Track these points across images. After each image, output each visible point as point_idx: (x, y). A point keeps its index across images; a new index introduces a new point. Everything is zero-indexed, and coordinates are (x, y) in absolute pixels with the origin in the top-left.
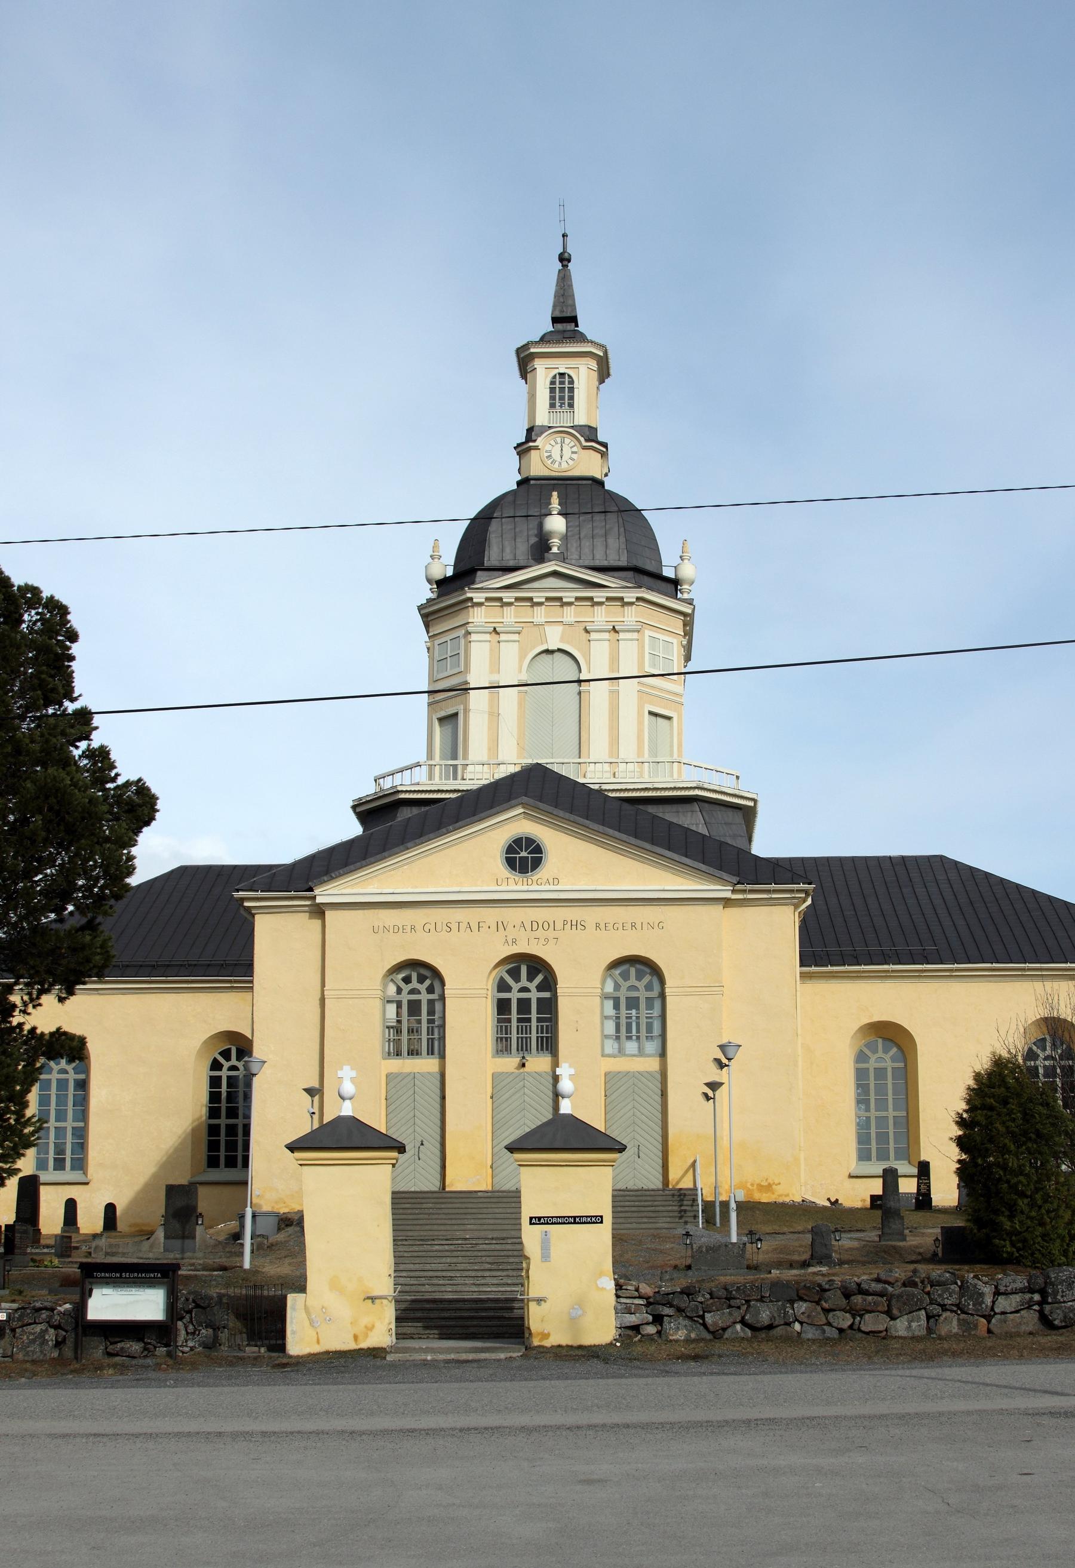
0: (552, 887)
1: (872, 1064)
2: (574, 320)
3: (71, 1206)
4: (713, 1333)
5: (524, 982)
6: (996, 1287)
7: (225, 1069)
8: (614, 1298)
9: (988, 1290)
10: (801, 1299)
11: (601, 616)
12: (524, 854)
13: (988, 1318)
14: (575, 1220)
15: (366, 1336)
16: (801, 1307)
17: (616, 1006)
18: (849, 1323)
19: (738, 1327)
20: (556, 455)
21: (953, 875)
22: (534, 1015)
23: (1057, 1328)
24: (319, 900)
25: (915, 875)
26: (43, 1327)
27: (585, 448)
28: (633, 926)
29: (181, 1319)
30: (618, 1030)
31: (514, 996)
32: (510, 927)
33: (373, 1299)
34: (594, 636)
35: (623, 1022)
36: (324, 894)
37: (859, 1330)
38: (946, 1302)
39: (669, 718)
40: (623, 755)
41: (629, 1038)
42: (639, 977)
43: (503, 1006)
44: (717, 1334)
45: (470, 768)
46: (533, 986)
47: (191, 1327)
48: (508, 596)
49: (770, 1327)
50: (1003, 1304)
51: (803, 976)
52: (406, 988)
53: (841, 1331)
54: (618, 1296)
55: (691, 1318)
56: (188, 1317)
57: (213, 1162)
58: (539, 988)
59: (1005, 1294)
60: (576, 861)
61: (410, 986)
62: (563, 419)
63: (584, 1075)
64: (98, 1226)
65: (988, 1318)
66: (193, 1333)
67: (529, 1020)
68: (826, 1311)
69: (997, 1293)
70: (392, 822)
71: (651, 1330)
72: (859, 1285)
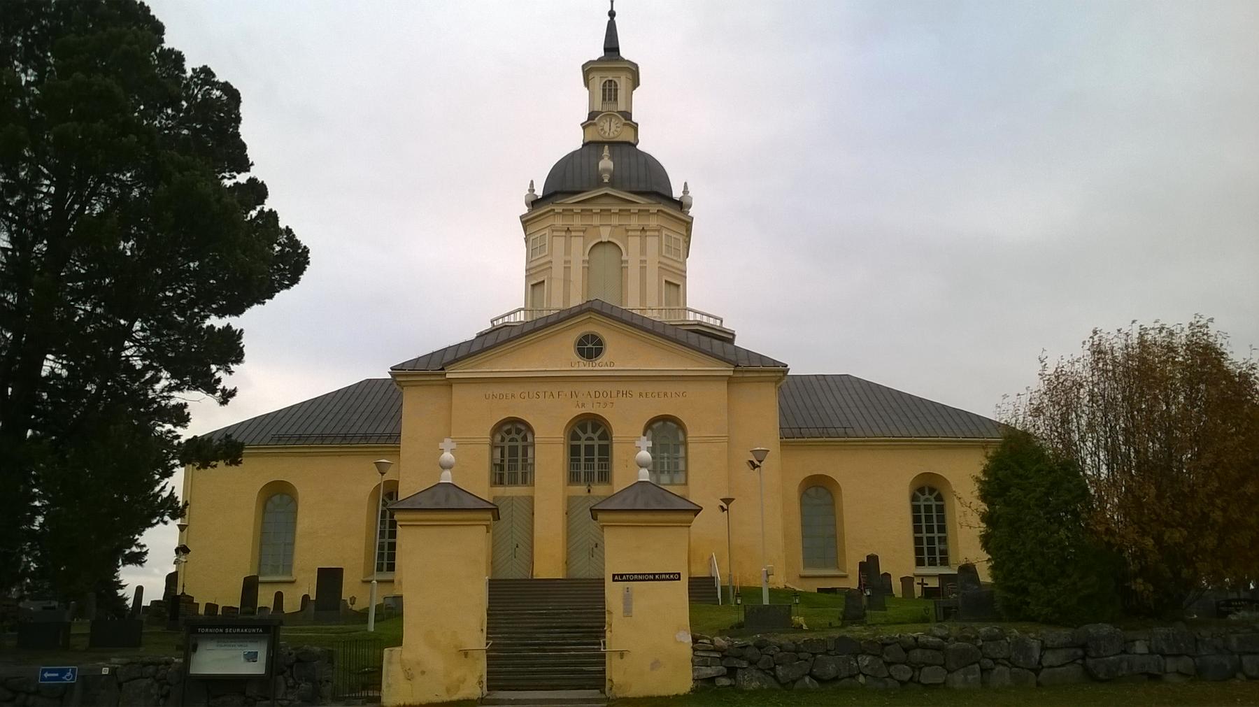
2: (617, 50)
3: (279, 597)
4: (783, 685)
5: (590, 434)
6: (1043, 642)
8: (691, 651)
9: (1035, 645)
10: (863, 653)
11: (635, 222)
13: (1037, 672)
14: (655, 577)
15: (458, 688)
16: (865, 660)
18: (909, 676)
19: (807, 679)
20: (607, 128)
21: (857, 385)
22: (596, 457)
23: (1101, 681)
24: (448, 376)
25: (832, 385)
26: (149, 681)
28: (665, 394)
29: (282, 673)
31: (583, 443)
33: (466, 654)
37: (919, 682)
38: (998, 655)
39: (678, 286)
40: (649, 304)
42: (666, 431)
43: (574, 451)
44: (787, 685)
45: (559, 243)
46: (595, 436)
47: (291, 681)
48: (577, 208)
49: (836, 679)
50: (1050, 658)
52: (508, 438)
53: (902, 683)
54: (694, 650)
55: (763, 670)
56: (289, 672)
58: (600, 438)
59: (1053, 649)
60: (622, 355)
62: (610, 107)
65: (1037, 672)
66: (293, 687)
67: (593, 460)
68: (889, 664)
69: (1044, 648)
70: (499, 338)
71: (725, 682)
72: (916, 639)
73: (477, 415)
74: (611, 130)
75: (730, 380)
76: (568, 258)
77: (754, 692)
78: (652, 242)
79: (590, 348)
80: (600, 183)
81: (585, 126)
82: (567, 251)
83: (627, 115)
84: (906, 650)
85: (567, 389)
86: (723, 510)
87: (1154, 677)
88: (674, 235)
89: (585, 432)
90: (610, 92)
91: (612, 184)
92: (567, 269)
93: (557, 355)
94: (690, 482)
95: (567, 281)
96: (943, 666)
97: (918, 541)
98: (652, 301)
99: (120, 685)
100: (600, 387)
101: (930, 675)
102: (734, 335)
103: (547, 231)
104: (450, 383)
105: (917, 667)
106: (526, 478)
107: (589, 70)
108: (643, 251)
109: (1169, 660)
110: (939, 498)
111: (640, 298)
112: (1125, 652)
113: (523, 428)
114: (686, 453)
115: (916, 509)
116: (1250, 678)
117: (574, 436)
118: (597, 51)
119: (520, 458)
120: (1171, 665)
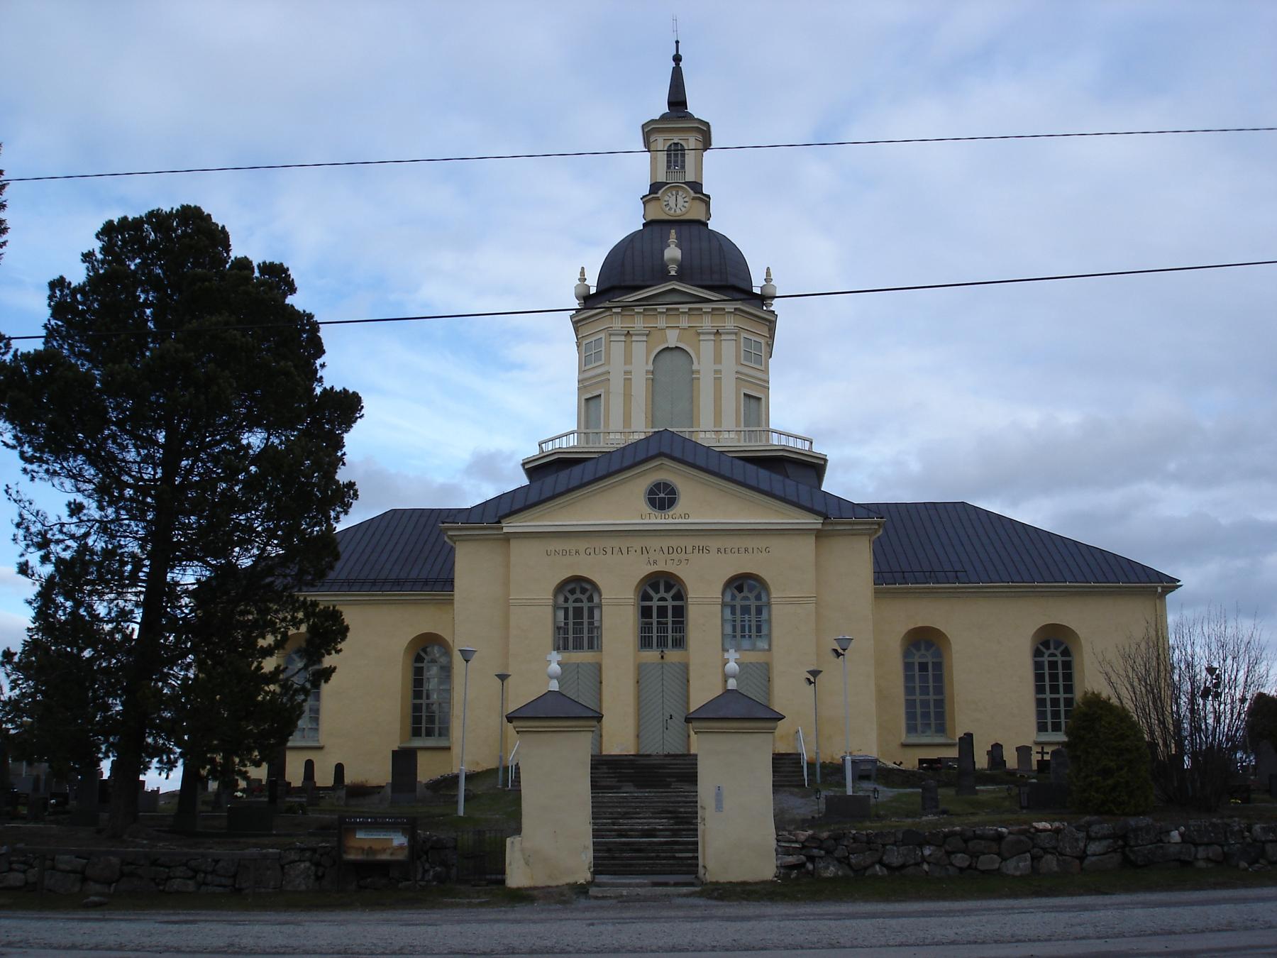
0: (684, 521)
1: (917, 660)
2: (684, 104)
3: (309, 765)
5: (662, 593)
7: (655, 599)
10: (929, 844)
11: (707, 323)
12: (662, 495)
17: (733, 613)
19: (877, 867)
20: (672, 203)
22: (670, 619)
24: (505, 530)
27: (694, 199)
28: (746, 550)
30: (734, 631)
31: (655, 604)
32: (651, 551)
34: (702, 337)
35: (738, 624)
36: (509, 526)
37: (976, 869)
39: (759, 399)
41: (743, 636)
43: (646, 612)
44: (860, 872)
45: (617, 349)
49: (903, 866)
50: (1094, 847)
51: (876, 592)
52: (571, 598)
53: (961, 869)
54: (778, 841)
57: (416, 732)
58: (674, 598)
60: (702, 504)
61: (575, 596)
63: (712, 662)
64: (329, 782)
70: (553, 474)
73: (535, 574)
74: (678, 206)
75: (819, 535)
76: (628, 368)
77: (834, 879)
78: (728, 347)
79: (662, 498)
80: (665, 277)
81: (646, 200)
82: (628, 359)
83: (696, 186)
84: (966, 841)
85: (637, 543)
86: (811, 683)
87: (1185, 864)
88: (753, 338)
89: (657, 592)
90: (676, 155)
91: (680, 277)
92: (628, 381)
93: (622, 505)
94: (774, 648)
95: (627, 396)
96: (998, 854)
97: (1040, 703)
98: (729, 421)
99: (282, 867)
100: (674, 542)
101: (988, 861)
102: (826, 460)
103: (602, 335)
104: (508, 538)
105: (974, 855)
106: (593, 644)
107: (650, 131)
108: (718, 358)
109: (1200, 849)
110: (1066, 652)
111: (717, 429)
112: (1161, 841)
113: (588, 586)
114: (770, 615)
115: (1038, 666)
116: (1271, 863)
117: (646, 597)
118: (659, 106)
119: (586, 620)
120: (1201, 852)
